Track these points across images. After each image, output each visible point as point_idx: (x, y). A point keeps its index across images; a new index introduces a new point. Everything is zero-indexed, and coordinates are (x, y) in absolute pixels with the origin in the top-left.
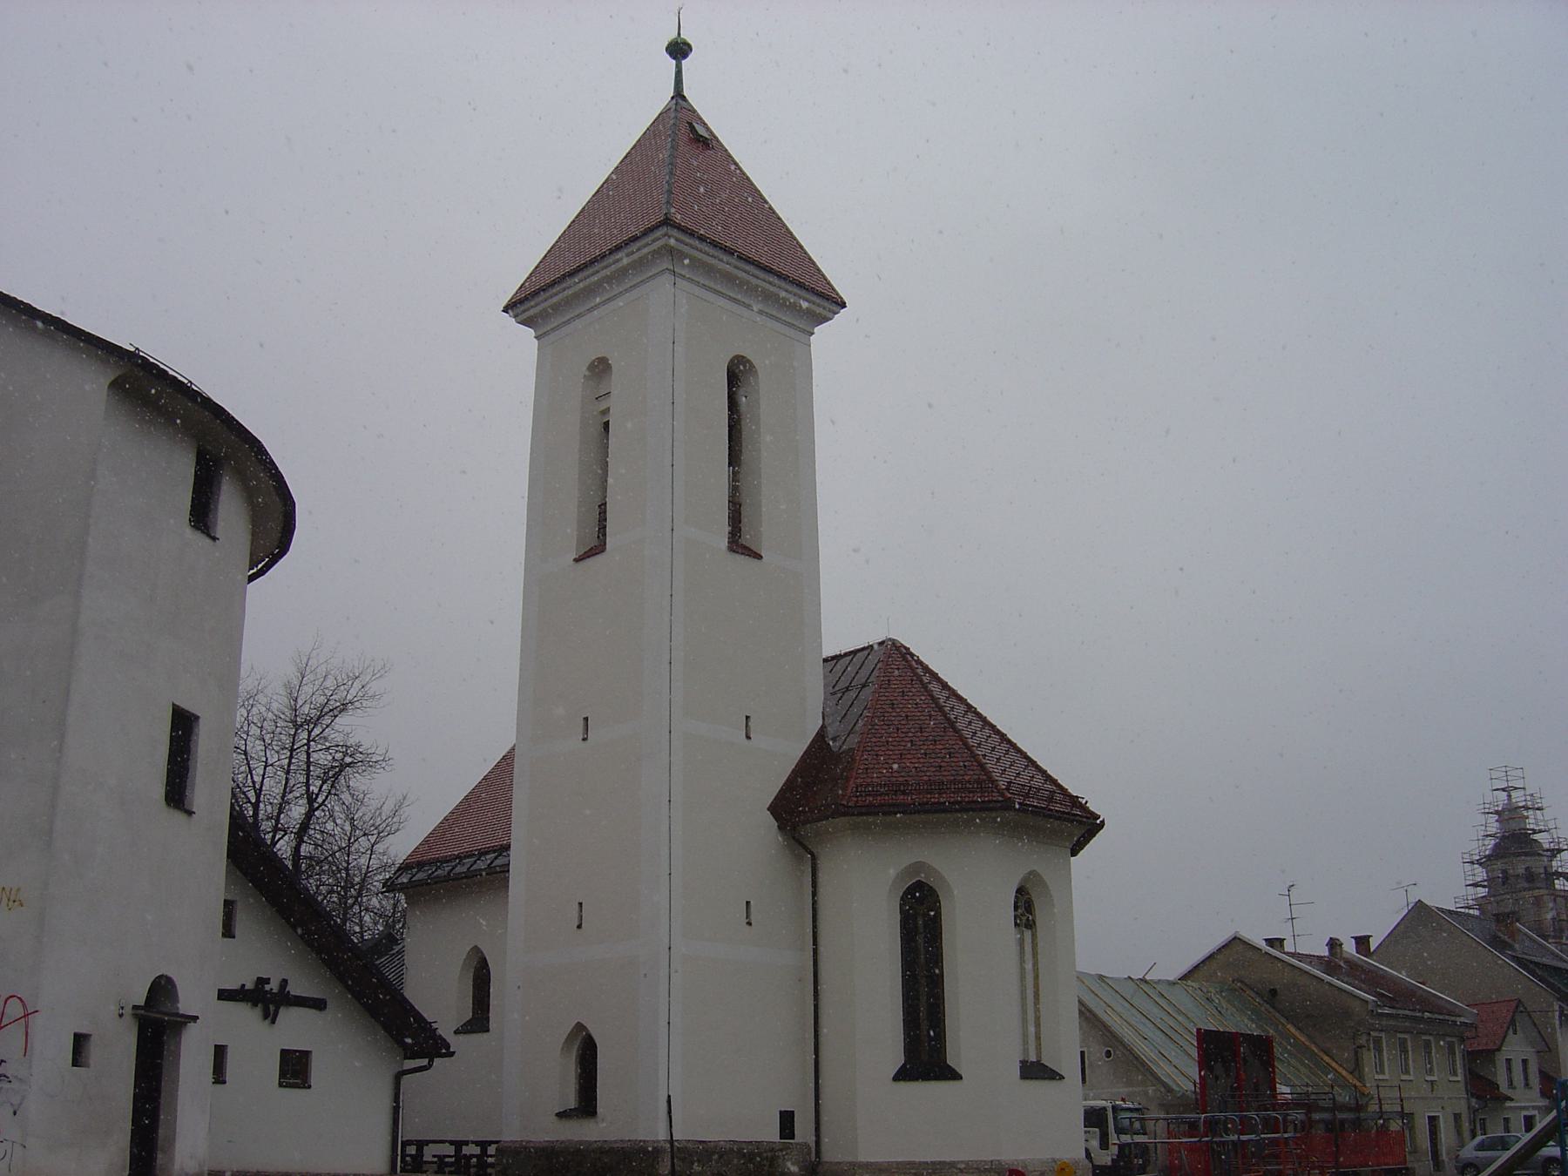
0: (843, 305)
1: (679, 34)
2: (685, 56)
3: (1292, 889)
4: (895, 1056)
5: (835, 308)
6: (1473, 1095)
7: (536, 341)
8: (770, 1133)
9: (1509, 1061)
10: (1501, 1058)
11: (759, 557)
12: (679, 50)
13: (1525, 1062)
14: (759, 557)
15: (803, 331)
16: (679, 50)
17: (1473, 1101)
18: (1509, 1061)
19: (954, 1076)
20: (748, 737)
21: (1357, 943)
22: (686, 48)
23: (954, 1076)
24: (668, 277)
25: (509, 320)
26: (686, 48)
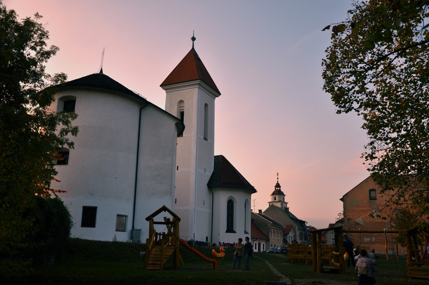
0: (220, 94)
1: (193, 36)
2: (195, 40)
3: (255, 201)
4: (225, 229)
5: (219, 95)
6: (284, 242)
7: (166, 93)
8: (205, 241)
9: (289, 236)
10: (288, 236)
11: (207, 140)
12: (193, 39)
13: (292, 237)
14: (207, 140)
15: (213, 98)
16: (193, 39)
17: (284, 244)
18: (289, 236)
19: (235, 232)
20: (205, 172)
21: (259, 211)
22: (195, 39)
23: (235, 232)
24: (197, 88)
25: (161, 88)
26: (195, 39)
